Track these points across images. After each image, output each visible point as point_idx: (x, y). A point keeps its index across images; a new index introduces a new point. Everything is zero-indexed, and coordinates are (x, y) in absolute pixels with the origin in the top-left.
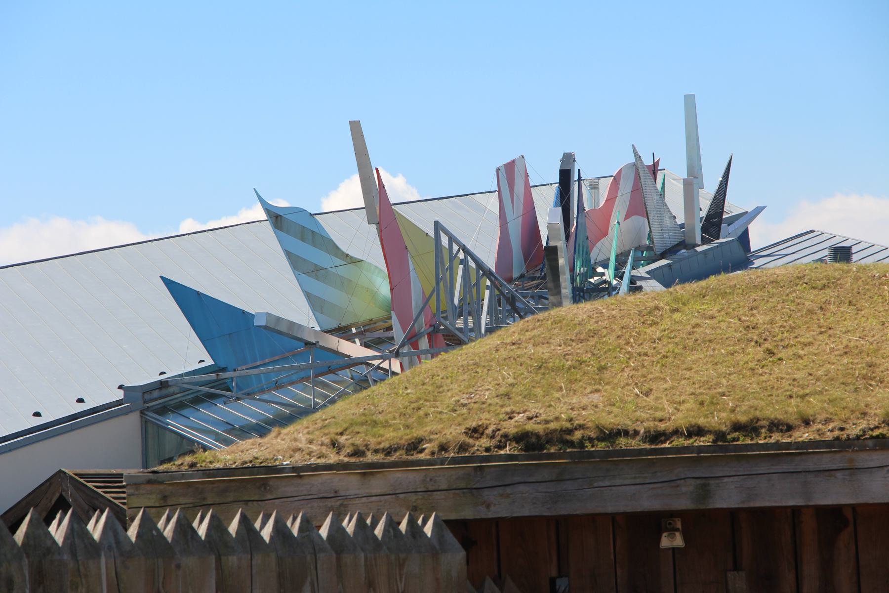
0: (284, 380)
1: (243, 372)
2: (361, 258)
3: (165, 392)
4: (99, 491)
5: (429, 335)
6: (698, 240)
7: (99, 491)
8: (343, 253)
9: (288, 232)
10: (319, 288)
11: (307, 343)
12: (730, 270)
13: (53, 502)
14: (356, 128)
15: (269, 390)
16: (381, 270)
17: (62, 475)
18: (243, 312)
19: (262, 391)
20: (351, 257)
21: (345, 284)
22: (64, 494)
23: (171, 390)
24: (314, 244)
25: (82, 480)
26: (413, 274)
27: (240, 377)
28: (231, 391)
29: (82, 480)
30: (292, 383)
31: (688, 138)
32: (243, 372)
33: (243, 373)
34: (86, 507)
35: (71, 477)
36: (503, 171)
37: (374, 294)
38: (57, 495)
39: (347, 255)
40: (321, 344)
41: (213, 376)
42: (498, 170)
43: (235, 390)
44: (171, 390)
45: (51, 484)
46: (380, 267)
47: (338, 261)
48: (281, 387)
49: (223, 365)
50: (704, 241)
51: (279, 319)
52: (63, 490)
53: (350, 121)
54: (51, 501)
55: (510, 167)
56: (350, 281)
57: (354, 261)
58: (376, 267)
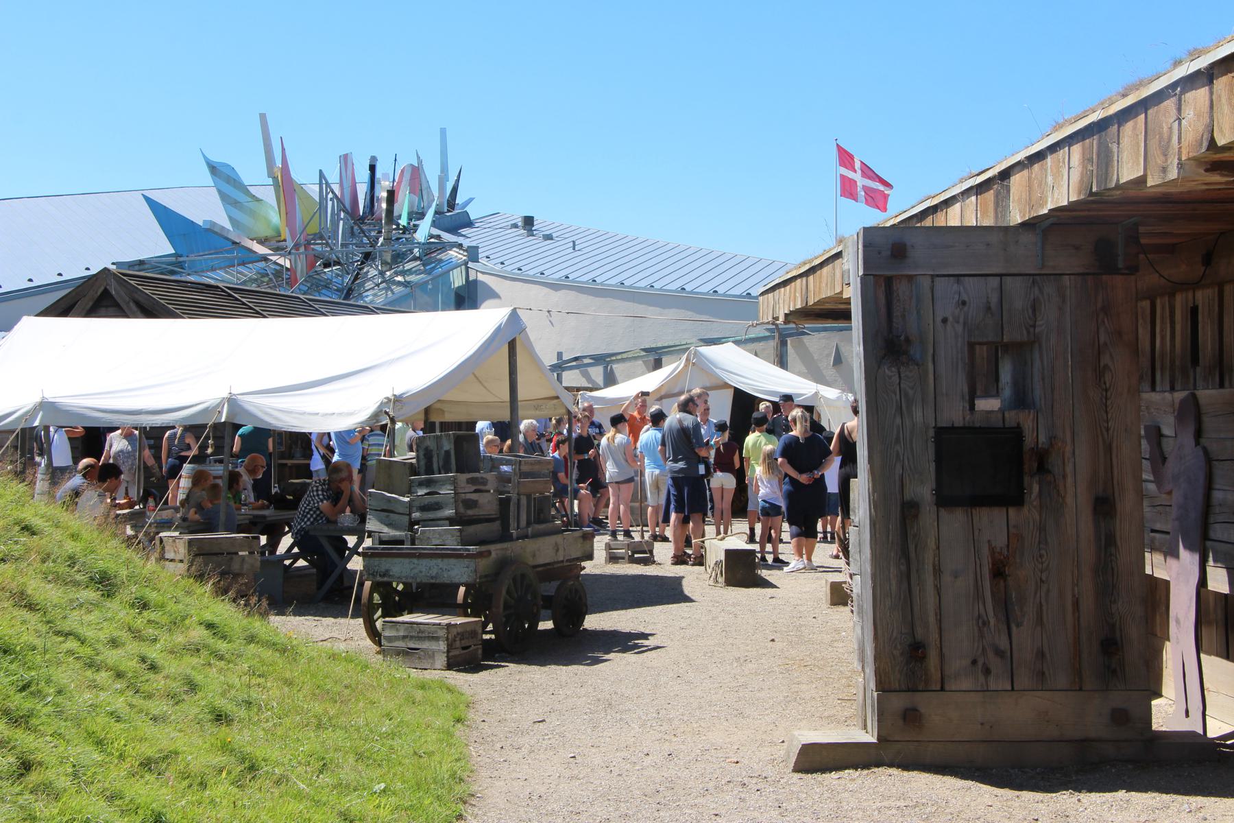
0: (217, 265)
1: (192, 257)
2: (261, 198)
3: (142, 267)
4: (140, 287)
5: (305, 245)
6: (446, 211)
7: (140, 287)
8: (252, 194)
9: (220, 178)
10: (239, 215)
11: (234, 243)
12: (343, 296)
13: (99, 294)
14: (263, 117)
15: (208, 271)
16: (273, 207)
17: (107, 272)
18: (192, 222)
19: (203, 271)
20: (256, 198)
21: (252, 213)
22: (108, 287)
23: (146, 266)
24: (235, 187)
25: (125, 278)
26: (297, 207)
27: (189, 261)
28: (184, 269)
29: (125, 278)
30: (220, 269)
31: (442, 152)
32: (192, 257)
33: (193, 258)
34: (127, 299)
35: (114, 274)
36: (342, 158)
37: (268, 222)
38: (102, 288)
39: (254, 196)
40: (243, 244)
41: (173, 259)
42: (340, 157)
43: (187, 269)
44: (146, 266)
45: (96, 280)
46: (273, 205)
47: (250, 199)
48: (215, 270)
49: (180, 253)
50: (449, 211)
51: (214, 224)
52: (107, 284)
53: (260, 114)
54: (96, 293)
55: (346, 156)
56: (255, 211)
57: (258, 200)
58: (271, 205)
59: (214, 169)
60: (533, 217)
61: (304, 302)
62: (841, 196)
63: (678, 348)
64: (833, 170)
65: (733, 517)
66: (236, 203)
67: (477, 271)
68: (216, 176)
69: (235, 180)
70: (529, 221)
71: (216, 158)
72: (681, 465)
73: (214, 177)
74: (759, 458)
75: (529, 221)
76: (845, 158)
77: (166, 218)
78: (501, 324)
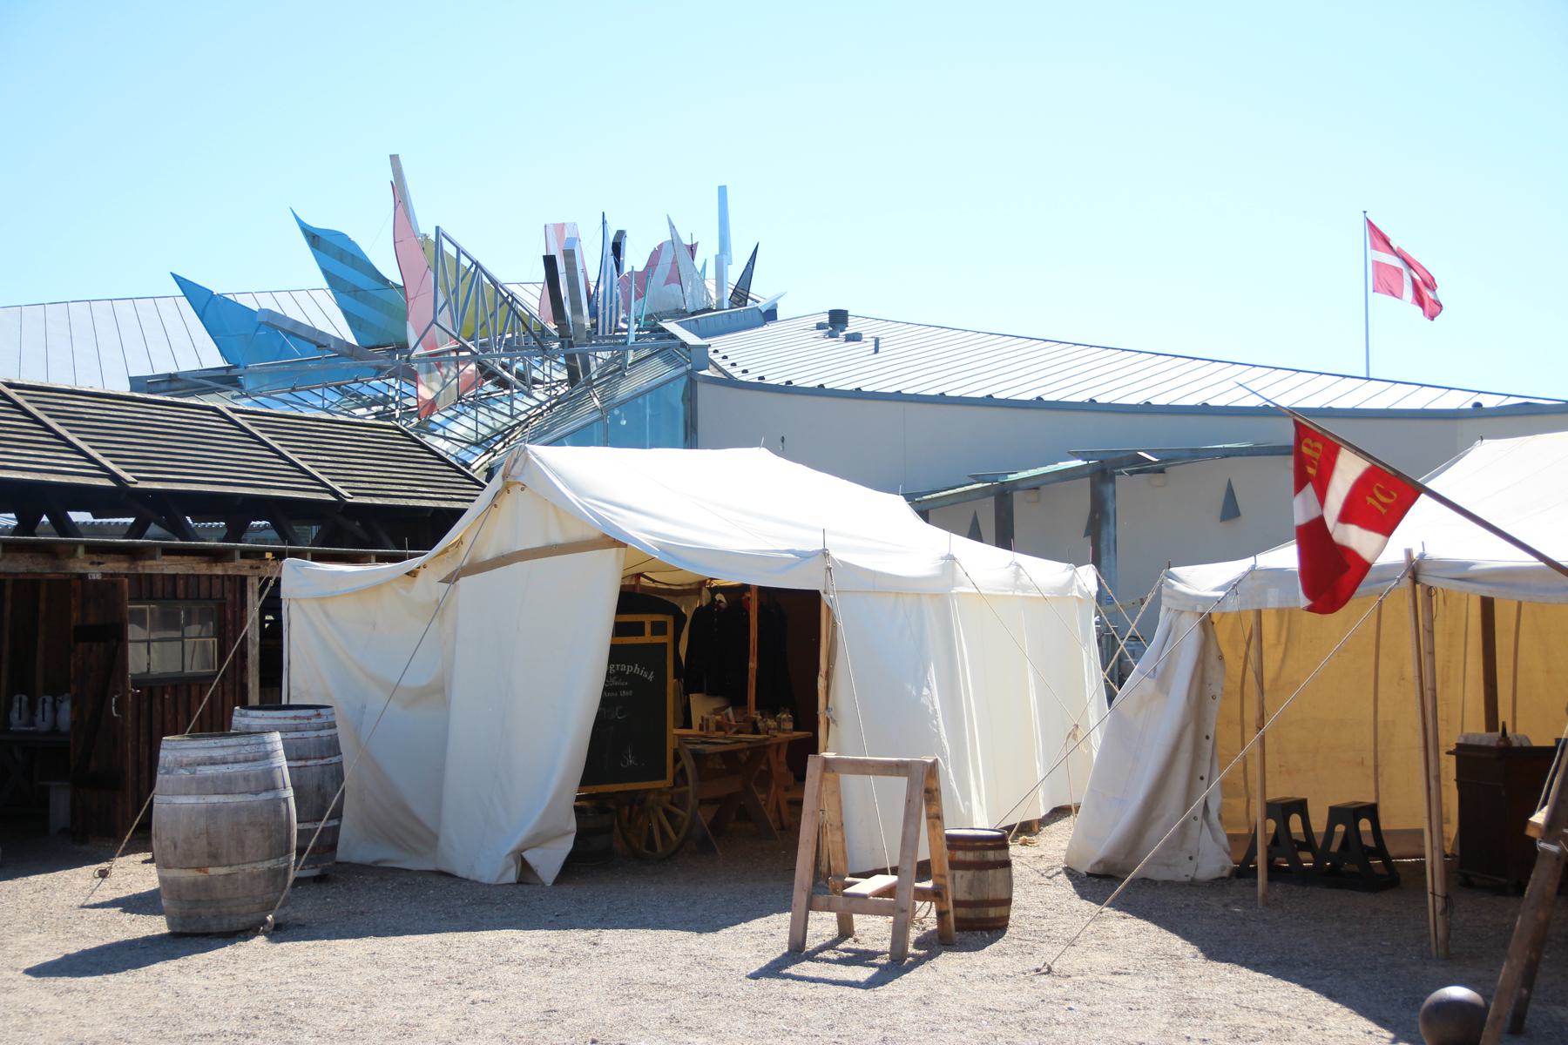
41: (224, 373)
59: (315, 238)
60: (847, 311)
61: (222, 415)
62: (1374, 291)
63: (182, 392)
64: (1356, 255)
65: (929, 860)
66: (356, 291)
67: (271, 292)
68: (319, 249)
69: (353, 255)
70: (838, 319)
71: (318, 222)
72: (636, 764)
73: (314, 250)
74: (288, 852)
75: (838, 319)
76: (1379, 238)
77: (207, 305)
78: (1473, 564)
